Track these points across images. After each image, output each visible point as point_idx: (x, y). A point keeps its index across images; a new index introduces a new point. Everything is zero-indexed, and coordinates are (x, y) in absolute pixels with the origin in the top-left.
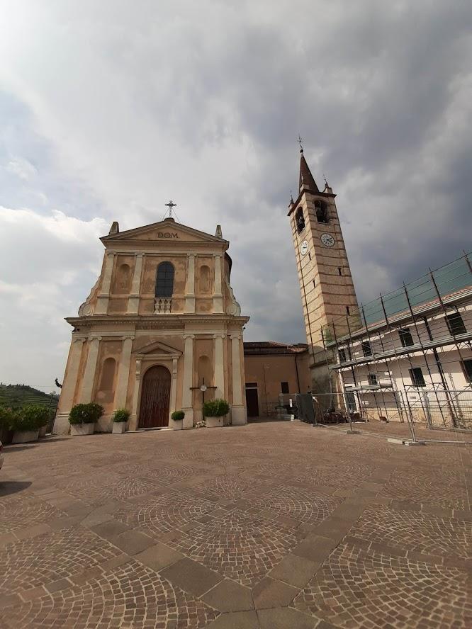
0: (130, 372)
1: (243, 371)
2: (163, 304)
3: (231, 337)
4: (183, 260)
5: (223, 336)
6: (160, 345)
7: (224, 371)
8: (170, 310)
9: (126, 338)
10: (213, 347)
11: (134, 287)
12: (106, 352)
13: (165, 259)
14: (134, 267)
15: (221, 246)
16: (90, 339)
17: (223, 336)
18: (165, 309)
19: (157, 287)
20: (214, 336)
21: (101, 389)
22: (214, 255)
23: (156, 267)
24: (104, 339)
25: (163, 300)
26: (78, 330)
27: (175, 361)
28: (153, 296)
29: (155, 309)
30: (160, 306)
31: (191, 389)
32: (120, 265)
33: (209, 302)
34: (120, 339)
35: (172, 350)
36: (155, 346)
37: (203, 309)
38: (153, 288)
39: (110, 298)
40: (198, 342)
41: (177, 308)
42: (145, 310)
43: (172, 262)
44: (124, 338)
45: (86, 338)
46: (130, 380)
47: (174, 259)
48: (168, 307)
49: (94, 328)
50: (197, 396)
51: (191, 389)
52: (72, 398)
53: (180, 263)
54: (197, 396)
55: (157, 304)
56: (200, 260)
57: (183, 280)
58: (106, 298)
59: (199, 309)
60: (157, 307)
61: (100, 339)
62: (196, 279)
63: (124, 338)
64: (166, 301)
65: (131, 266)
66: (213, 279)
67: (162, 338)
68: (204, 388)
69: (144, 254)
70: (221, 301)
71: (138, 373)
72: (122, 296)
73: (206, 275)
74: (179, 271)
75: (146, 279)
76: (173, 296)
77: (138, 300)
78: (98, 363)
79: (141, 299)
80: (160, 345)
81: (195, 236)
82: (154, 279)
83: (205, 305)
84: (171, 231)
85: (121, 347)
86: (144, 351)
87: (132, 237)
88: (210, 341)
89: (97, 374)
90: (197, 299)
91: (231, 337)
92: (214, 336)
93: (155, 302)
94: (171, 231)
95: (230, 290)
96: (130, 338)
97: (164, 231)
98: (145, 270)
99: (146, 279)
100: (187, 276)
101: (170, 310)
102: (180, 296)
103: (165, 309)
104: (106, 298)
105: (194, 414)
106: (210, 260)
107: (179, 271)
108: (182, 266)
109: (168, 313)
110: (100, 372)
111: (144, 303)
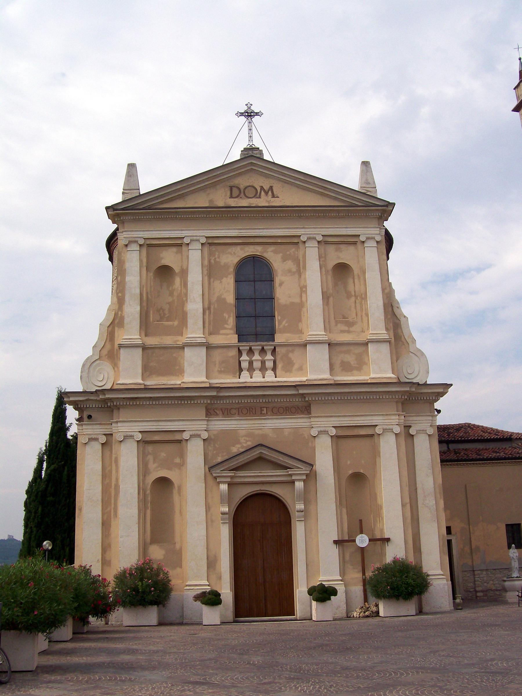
0: (208, 508)
1: (442, 503)
2: (257, 357)
3: (412, 431)
4: (292, 250)
5: (397, 429)
6: (265, 451)
7: (403, 505)
8: (274, 369)
9: (192, 436)
10: (375, 453)
11: (190, 321)
12: (152, 466)
13: (250, 251)
14: (184, 272)
15: (379, 214)
16: (119, 437)
17: (397, 429)
18: (263, 369)
19: (238, 317)
20: (378, 430)
21: (154, 540)
22: (362, 238)
23: (231, 269)
24: (341, 433)
25: (256, 346)
26: (90, 417)
27: (299, 485)
28: (234, 339)
29: (241, 370)
30: (251, 363)
31: (336, 542)
32: (155, 267)
33: (359, 350)
34: (178, 437)
35: (291, 462)
36: (255, 453)
37: (347, 368)
38: (231, 321)
39: (145, 348)
40: (342, 442)
41: (289, 367)
42: (220, 372)
43: (265, 255)
44: (186, 436)
45: (109, 435)
46: (209, 522)
47: (272, 248)
48: (269, 364)
49: (123, 414)
50: (347, 557)
51: (336, 542)
52: (100, 557)
53: (284, 259)
54: (347, 557)
55: (245, 357)
56: (331, 249)
57: (297, 300)
58: (200, 345)
59: (337, 367)
60: (245, 365)
61: (139, 437)
62: (326, 297)
63: (186, 436)
64: (263, 351)
65: (177, 269)
66: (364, 297)
67: (264, 436)
68: (362, 541)
69: (203, 240)
70: (385, 349)
71: (226, 509)
72: (168, 340)
73: (345, 285)
74: (283, 278)
75: (214, 299)
76: (279, 338)
77: (203, 351)
78: (141, 489)
79: (209, 347)
80: (265, 451)
81: (322, 194)
82: (231, 298)
83: (350, 359)
84: (259, 182)
85: (182, 455)
86: (234, 463)
87: (162, 203)
88: (366, 442)
89: (142, 511)
90: (145, 348)
91: (412, 431)
92: (378, 430)
93: (240, 353)
94: (259, 182)
95: (402, 320)
96: (199, 436)
97: (243, 182)
98: (210, 277)
99: (214, 299)
100: (303, 289)
101: (274, 369)
102: (294, 339)
103: (263, 369)
104: (200, 345)
105: (516, 602)
106: (352, 248)
107: (283, 278)
108: (290, 265)
109: (270, 378)
110: (146, 508)
111: (217, 355)
